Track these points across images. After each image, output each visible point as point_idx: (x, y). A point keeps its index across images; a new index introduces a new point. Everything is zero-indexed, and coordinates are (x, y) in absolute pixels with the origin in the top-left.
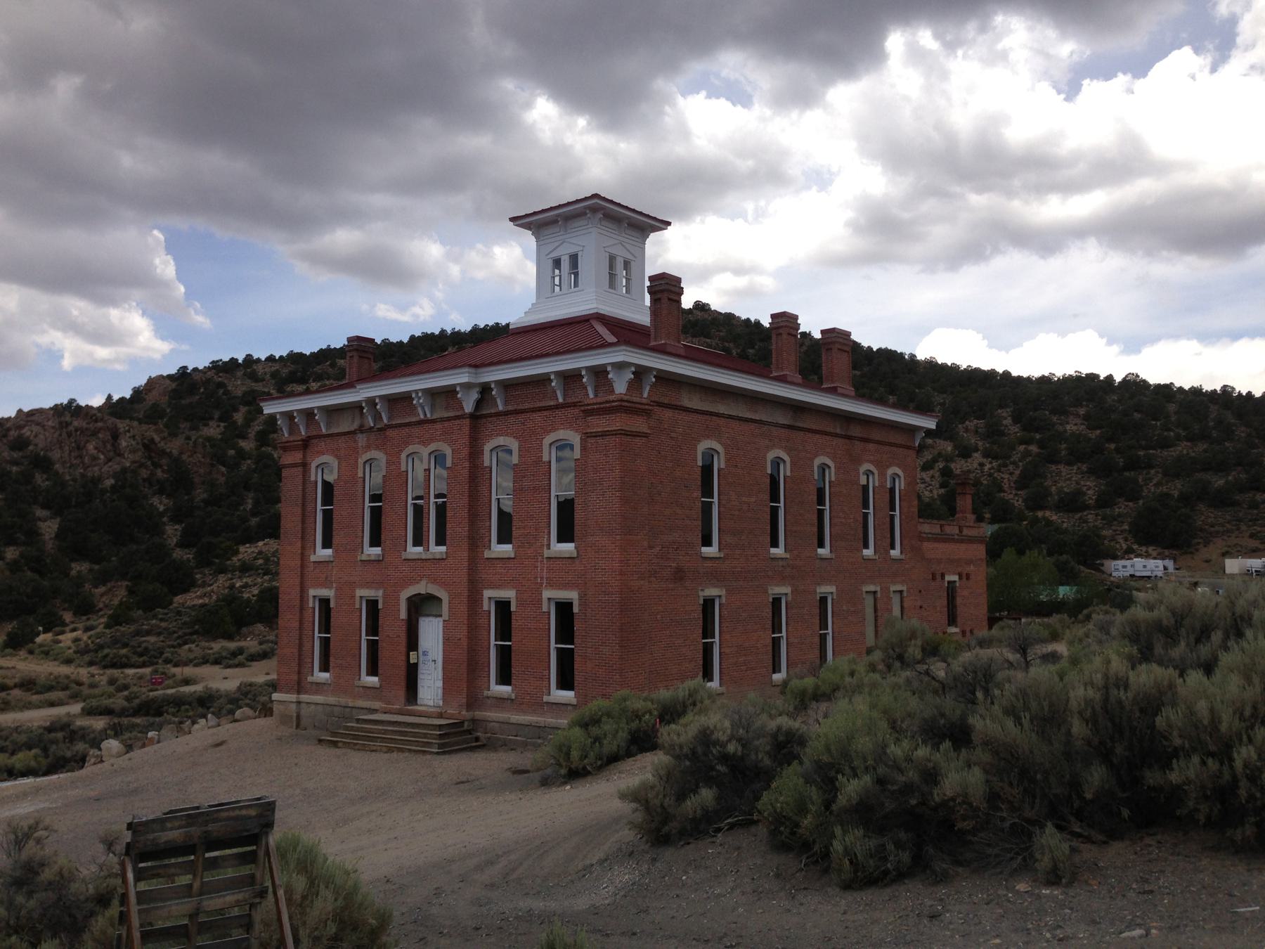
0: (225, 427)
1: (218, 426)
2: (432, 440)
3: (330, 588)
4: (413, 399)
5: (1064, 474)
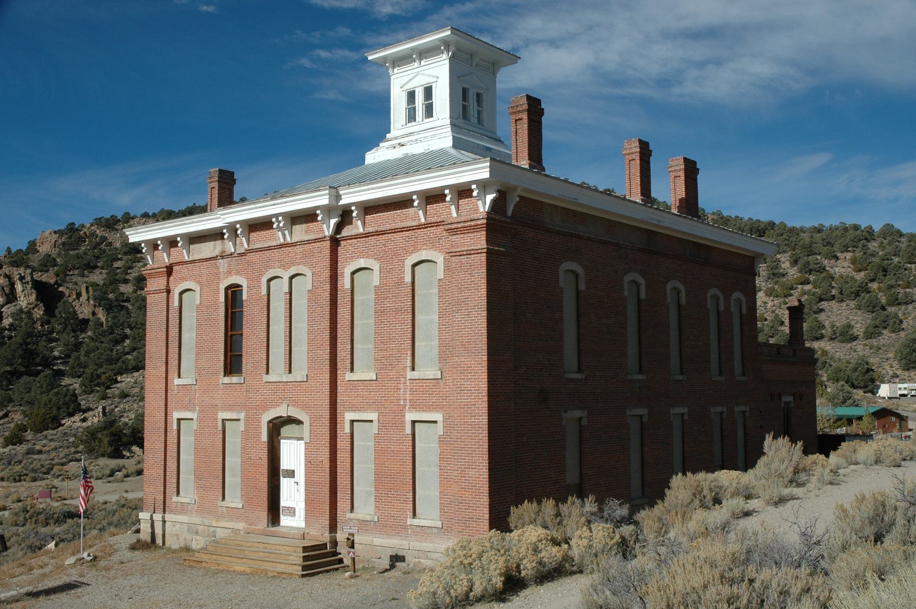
0: (107, 274)
1: (101, 273)
2: (293, 263)
3: (193, 410)
4: (273, 223)
5: (835, 310)
